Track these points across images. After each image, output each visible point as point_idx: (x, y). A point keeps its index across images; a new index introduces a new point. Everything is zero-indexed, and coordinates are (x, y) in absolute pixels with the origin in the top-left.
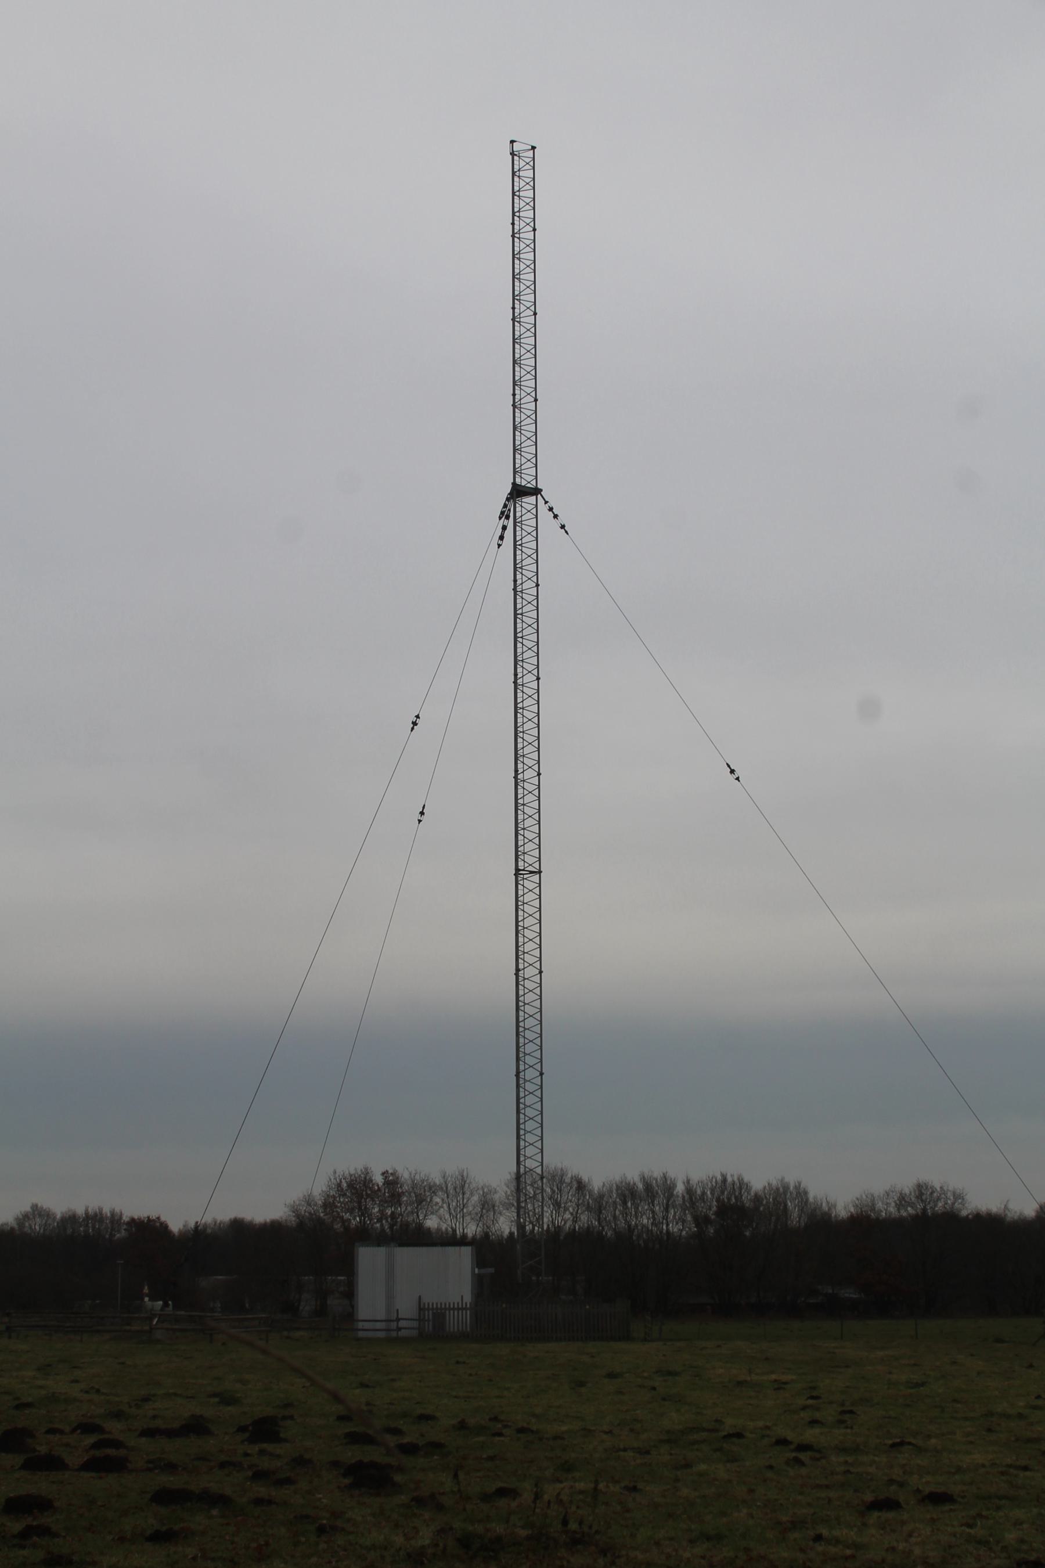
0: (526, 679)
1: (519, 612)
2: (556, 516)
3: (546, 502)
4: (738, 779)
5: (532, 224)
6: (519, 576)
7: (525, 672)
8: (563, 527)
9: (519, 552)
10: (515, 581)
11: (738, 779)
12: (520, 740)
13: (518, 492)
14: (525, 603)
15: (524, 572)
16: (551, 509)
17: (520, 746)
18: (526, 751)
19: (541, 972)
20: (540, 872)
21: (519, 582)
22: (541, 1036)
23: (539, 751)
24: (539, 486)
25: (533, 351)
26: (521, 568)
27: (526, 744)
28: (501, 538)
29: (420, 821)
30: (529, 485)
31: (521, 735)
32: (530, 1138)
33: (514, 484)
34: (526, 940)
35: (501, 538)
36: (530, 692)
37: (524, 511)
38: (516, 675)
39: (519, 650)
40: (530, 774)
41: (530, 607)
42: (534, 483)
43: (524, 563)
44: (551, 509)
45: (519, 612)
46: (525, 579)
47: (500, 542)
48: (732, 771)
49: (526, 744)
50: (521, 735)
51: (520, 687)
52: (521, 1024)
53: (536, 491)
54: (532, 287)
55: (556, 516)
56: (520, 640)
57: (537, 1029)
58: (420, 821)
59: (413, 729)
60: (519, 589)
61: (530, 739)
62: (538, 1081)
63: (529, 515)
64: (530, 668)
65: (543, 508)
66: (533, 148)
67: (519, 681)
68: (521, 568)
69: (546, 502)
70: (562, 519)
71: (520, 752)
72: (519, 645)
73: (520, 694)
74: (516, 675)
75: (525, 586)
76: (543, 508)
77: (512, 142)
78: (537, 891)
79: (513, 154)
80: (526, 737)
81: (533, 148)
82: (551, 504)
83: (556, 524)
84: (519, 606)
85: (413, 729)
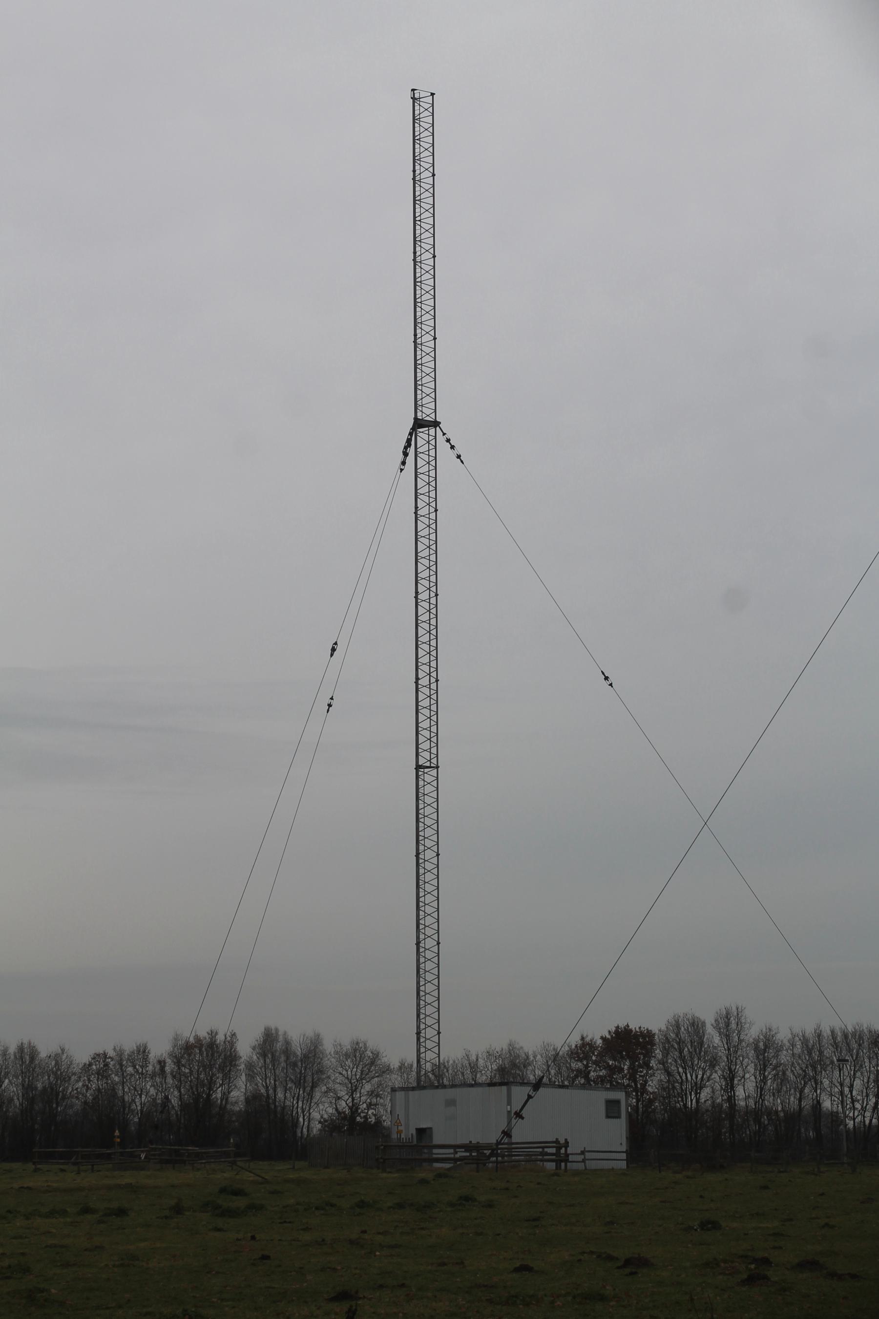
0: (424, 339)
1: (418, 280)
2: (452, 447)
3: (444, 434)
4: (611, 685)
5: (431, 169)
6: (417, 167)
7: (424, 333)
8: (459, 457)
9: (417, 146)
10: (414, 171)
11: (611, 685)
12: (419, 392)
13: (419, 424)
14: (423, 272)
15: (422, 184)
16: (448, 441)
17: (419, 397)
18: (425, 401)
19: (438, 943)
20: (437, 767)
21: (418, 253)
22: (438, 822)
23: (433, 135)
24: (438, 420)
25: (431, 210)
26: (420, 241)
27: (424, 395)
28: (404, 463)
29: (332, 699)
30: (428, 419)
31: (420, 387)
32: (429, 1021)
33: (416, 419)
34: (424, 375)
35: (404, 463)
36: (428, 350)
37: (423, 190)
38: (415, 335)
39: (418, 314)
40: (429, 854)
41: (427, 235)
42: (433, 416)
43: (422, 156)
44: (448, 441)
45: (418, 280)
46: (423, 272)
47: (402, 467)
48: (606, 678)
49: (424, 395)
50: (419, 284)
51: (419, 346)
52: (422, 988)
53: (436, 424)
54: (431, 110)
55: (452, 447)
56: (419, 304)
57: (436, 993)
58: (332, 699)
59: (328, 711)
60: (418, 259)
61: (428, 391)
62: (435, 861)
63: (427, 113)
64: (428, 329)
65: (441, 439)
66: (433, 94)
67: (419, 341)
68: (420, 241)
69: (444, 434)
70: (459, 450)
71: (419, 403)
72: (418, 227)
73: (418, 270)
74: (415, 335)
75: (423, 176)
76: (441, 439)
77: (413, 90)
78: (432, 312)
79: (414, 99)
80: (424, 389)
81: (433, 94)
82: (448, 436)
83: (452, 454)
84: (418, 275)
85: (328, 711)
